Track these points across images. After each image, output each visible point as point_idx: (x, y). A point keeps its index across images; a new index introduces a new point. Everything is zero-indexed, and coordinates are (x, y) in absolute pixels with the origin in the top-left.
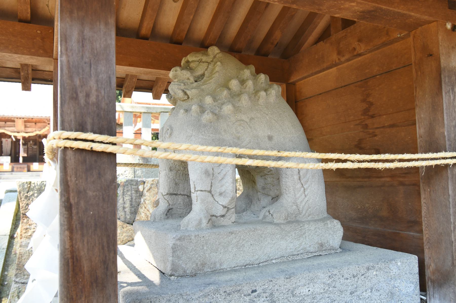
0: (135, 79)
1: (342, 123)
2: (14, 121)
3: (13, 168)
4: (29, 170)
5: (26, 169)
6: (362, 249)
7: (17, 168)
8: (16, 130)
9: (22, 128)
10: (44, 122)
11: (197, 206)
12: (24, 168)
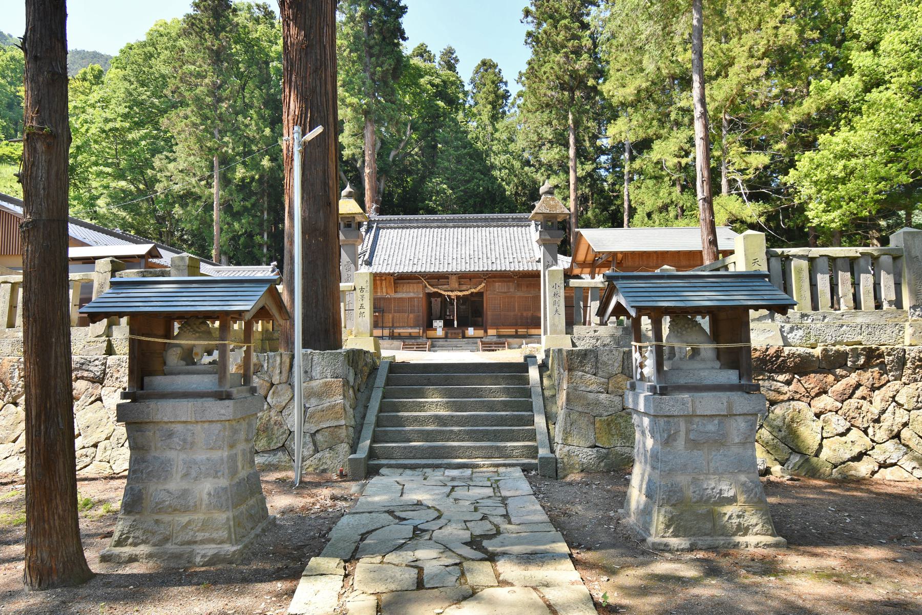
0: (242, 70)
1: (837, 435)
2: (448, 278)
3: (446, 334)
4: (464, 337)
5: (461, 335)
6: (796, 99)
7: (452, 334)
8: (449, 289)
9: (457, 286)
10: (480, 277)
11: (677, 356)
12: (458, 334)
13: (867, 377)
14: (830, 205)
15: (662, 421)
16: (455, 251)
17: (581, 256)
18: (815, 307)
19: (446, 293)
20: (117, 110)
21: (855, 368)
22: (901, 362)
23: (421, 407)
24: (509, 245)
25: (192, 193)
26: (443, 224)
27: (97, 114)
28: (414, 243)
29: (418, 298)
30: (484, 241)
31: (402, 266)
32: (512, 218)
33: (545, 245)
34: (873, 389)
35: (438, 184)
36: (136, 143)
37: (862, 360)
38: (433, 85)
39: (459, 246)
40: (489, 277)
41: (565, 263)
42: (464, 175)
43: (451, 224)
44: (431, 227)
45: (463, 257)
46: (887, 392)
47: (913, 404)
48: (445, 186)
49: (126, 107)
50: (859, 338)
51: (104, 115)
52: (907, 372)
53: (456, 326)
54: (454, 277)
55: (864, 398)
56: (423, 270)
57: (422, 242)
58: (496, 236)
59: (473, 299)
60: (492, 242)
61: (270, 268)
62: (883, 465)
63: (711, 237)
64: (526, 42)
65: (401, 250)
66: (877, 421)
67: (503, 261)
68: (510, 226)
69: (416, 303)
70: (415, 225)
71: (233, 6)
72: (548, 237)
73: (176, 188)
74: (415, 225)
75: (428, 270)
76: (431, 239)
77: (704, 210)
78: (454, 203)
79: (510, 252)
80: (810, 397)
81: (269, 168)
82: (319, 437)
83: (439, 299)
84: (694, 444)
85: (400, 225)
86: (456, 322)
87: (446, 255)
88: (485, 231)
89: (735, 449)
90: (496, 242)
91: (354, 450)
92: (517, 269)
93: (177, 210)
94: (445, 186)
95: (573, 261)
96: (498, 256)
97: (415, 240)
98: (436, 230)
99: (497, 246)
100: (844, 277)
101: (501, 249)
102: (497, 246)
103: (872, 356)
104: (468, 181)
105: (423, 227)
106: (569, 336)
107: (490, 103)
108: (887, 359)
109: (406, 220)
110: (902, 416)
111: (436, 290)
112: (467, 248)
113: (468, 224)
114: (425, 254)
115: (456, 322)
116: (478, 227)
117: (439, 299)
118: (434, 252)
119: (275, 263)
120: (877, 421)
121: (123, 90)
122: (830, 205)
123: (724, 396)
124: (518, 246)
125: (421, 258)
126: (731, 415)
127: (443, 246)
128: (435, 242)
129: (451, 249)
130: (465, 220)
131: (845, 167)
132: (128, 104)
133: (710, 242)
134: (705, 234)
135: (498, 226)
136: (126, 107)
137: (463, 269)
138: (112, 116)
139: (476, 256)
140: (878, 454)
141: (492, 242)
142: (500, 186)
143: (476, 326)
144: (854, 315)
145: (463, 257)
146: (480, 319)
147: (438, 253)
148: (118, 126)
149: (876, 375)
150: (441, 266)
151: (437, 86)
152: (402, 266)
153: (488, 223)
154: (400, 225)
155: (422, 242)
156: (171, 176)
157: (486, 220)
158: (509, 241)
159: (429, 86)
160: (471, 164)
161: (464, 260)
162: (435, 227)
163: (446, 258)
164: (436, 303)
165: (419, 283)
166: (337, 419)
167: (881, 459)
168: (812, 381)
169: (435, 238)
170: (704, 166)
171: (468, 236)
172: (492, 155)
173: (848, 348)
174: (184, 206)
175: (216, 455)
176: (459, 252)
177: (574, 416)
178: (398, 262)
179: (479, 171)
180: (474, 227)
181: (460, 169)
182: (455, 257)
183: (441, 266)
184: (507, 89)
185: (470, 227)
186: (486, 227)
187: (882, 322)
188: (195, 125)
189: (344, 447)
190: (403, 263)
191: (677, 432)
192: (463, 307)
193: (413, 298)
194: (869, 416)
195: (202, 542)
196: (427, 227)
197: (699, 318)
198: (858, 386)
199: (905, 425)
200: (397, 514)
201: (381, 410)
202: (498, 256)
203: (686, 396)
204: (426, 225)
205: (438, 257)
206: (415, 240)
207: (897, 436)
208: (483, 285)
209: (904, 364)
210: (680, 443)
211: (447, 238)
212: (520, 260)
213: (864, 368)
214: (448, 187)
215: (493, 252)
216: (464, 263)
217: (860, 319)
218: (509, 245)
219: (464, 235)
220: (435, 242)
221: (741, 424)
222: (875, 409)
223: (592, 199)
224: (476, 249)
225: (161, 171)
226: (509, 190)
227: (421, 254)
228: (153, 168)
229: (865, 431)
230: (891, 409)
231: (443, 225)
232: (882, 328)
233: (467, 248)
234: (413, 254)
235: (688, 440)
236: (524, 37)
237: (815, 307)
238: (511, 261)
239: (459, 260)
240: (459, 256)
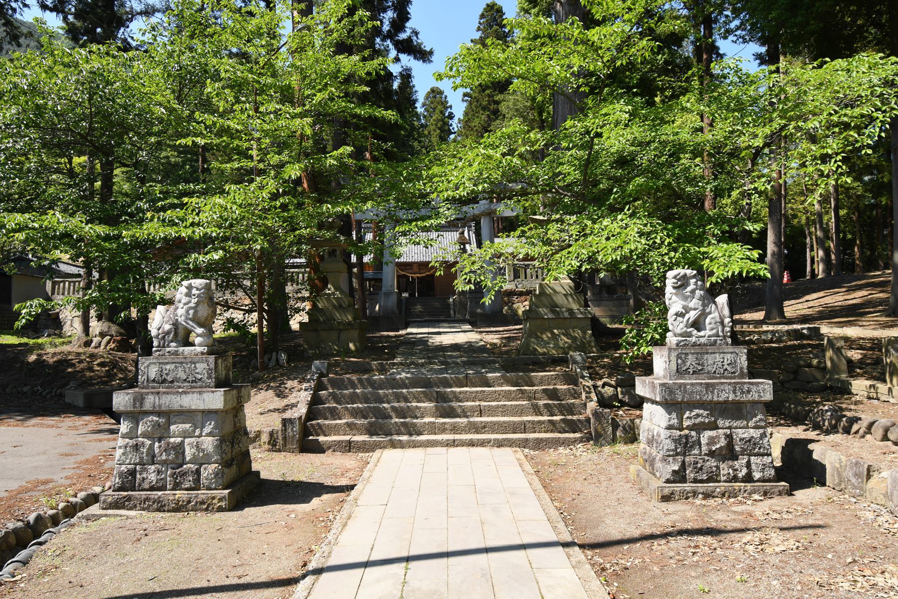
18: (526, 278)
64: (463, 100)
71: (437, 264)
80: (523, 302)
83: (405, 280)
100: (72, 284)
106: (646, 406)
107: (439, 128)
117: (405, 280)
168: (523, 298)
200: (309, 579)
236: (461, 97)
237: (526, 278)
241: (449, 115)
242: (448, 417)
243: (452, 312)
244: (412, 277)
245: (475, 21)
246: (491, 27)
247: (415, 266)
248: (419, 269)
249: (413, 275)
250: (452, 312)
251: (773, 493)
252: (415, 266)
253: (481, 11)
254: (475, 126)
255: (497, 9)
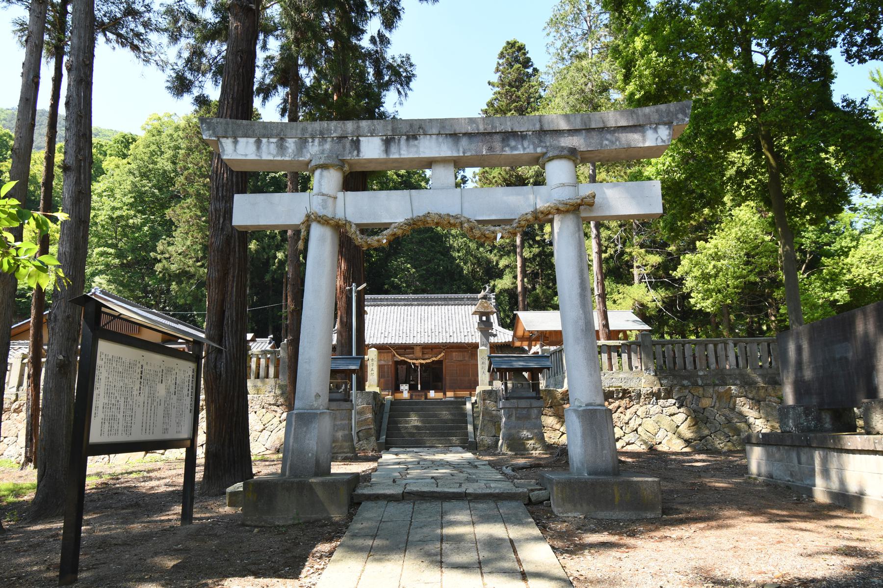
7: (416, 396)
9: (420, 355)
10: (440, 348)
13: (623, 403)
14: (707, 293)
15: (507, 410)
16: (419, 325)
17: (520, 333)
19: (411, 361)
20: (123, 200)
21: (618, 399)
22: (639, 395)
23: (407, 422)
24: (464, 320)
25: (186, 271)
26: (409, 303)
27: (108, 203)
28: (385, 319)
29: (388, 365)
30: (443, 317)
31: (375, 339)
32: (467, 298)
33: (481, 331)
34: (626, 408)
35: (403, 263)
36: (139, 228)
37: (621, 395)
38: (398, 175)
39: (423, 322)
40: (448, 348)
41: (506, 336)
42: (426, 256)
43: (416, 303)
44: (399, 305)
45: (426, 331)
46: (633, 410)
47: (644, 415)
48: (409, 266)
49: (131, 197)
50: (620, 384)
51: (112, 204)
52: (642, 400)
53: (419, 389)
54: (418, 348)
55: (622, 413)
56: (393, 342)
57: (392, 318)
58: (453, 313)
59: (434, 366)
60: (450, 318)
61: (268, 340)
62: (628, 444)
63: (604, 322)
65: (374, 325)
66: (627, 423)
67: (459, 335)
68: (465, 305)
69: (386, 370)
70: (385, 303)
72: (483, 327)
73: (174, 267)
74: (385, 303)
75: (396, 342)
76: (399, 316)
77: (599, 302)
78: (417, 281)
79: (465, 327)
81: (256, 250)
82: (360, 434)
83: (405, 367)
84: (518, 418)
85: (372, 303)
86: (419, 386)
87: (412, 329)
88: (444, 309)
89: (533, 420)
90: (454, 318)
91: (378, 439)
92: (470, 342)
93: (174, 286)
94: (409, 266)
95: (514, 336)
96: (455, 330)
97: (385, 316)
98: (403, 307)
99: (454, 322)
101: (458, 325)
102: (454, 322)
103: (625, 393)
104: (430, 261)
105: (392, 305)
108: (633, 394)
109: (378, 299)
110: (639, 421)
111: (403, 358)
112: (429, 323)
113: (430, 303)
114: (394, 328)
115: (419, 386)
116: (439, 305)
117: (405, 367)
118: (401, 327)
119: (272, 336)
120: (627, 423)
121: (129, 183)
122: (707, 293)
123: (528, 401)
124: (471, 322)
125: (390, 331)
126: (531, 408)
127: (409, 322)
128: (402, 318)
129: (416, 324)
130: (428, 299)
131: (714, 266)
132: (134, 195)
133: (604, 326)
134: (600, 319)
135: (455, 305)
136: (131, 197)
137: (426, 342)
138: (119, 205)
139: (437, 330)
140: (626, 439)
141: (450, 318)
142: (458, 265)
143: (437, 389)
144: (618, 373)
145: (426, 331)
146: (440, 384)
147: (405, 328)
148: (124, 214)
149: (628, 402)
150: (408, 338)
151: (402, 176)
152: (375, 339)
153: (446, 302)
154: (372, 303)
155: (392, 318)
156: (170, 258)
157: (445, 299)
158: (464, 317)
159: (395, 177)
160: (432, 246)
161: (426, 334)
162: (402, 305)
163: (412, 331)
164: (402, 369)
165: (388, 352)
166: (369, 425)
167: (627, 441)
169: (402, 315)
170: (598, 272)
171: (430, 313)
172: (451, 237)
173: (614, 389)
174: (179, 283)
175: (344, 422)
176: (423, 327)
177: (486, 422)
178: (372, 336)
179: (439, 252)
180: (435, 305)
181: (422, 251)
182: (419, 331)
183: (408, 338)
184: (465, 174)
185: (432, 305)
186: (445, 305)
187: (632, 377)
188: (199, 217)
189: (373, 439)
190: (376, 336)
191: (512, 414)
192: (425, 374)
193: (384, 365)
194: (624, 421)
195: (340, 453)
196: (395, 305)
197: (524, 373)
198: (619, 407)
199: (640, 425)
201: (388, 424)
202: (455, 330)
203: (515, 401)
204: (395, 303)
205: (405, 331)
206: (385, 316)
207: (636, 430)
208: (443, 354)
209: (640, 396)
210: (513, 418)
211: (413, 315)
212: (473, 333)
213: (622, 398)
214: (412, 266)
215: (451, 327)
216: (426, 336)
217: (621, 376)
218: (464, 320)
219: (426, 312)
220: (402, 318)
221: (535, 411)
222: (626, 418)
223: (542, 276)
224: (437, 324)
225: (162, 253)
226: (466, 269)
227: (391, 328)
228: (156, 251)
229: (621, 428)
230: (634, 418)
231: (408, 303)
232: (631, 379)
233: (429, 323)
234: (384, 329)
235: (516, 417)
238: (466, 334)
239: (423, 333)
240: (422, 330)
241: (462, 179)
242: (311, 413)
243: (470, 428)
244: (413, 364)
245: (493, 60)
246: (512, 66)
247: (418, 350)
248: (423, 354)
249: (415, 361)
250: (470, 428)
251: (259, 573)
252: (418, 350)
253: (500, 49)
254: (494, 177)
255: (519, 47)
